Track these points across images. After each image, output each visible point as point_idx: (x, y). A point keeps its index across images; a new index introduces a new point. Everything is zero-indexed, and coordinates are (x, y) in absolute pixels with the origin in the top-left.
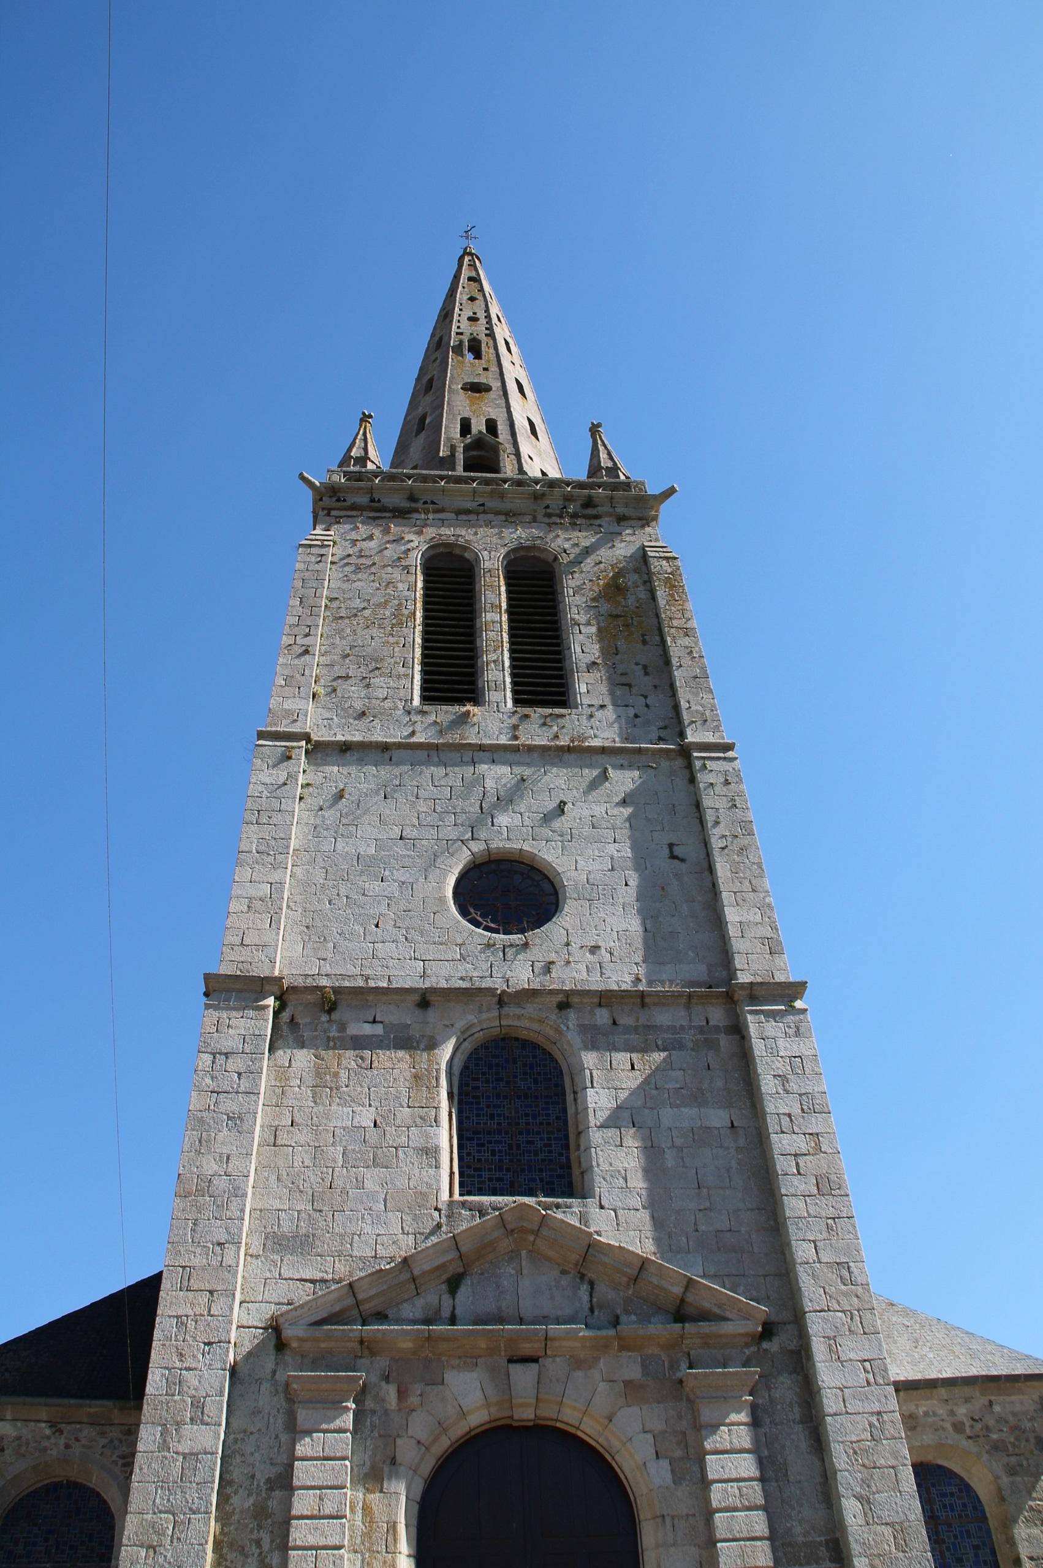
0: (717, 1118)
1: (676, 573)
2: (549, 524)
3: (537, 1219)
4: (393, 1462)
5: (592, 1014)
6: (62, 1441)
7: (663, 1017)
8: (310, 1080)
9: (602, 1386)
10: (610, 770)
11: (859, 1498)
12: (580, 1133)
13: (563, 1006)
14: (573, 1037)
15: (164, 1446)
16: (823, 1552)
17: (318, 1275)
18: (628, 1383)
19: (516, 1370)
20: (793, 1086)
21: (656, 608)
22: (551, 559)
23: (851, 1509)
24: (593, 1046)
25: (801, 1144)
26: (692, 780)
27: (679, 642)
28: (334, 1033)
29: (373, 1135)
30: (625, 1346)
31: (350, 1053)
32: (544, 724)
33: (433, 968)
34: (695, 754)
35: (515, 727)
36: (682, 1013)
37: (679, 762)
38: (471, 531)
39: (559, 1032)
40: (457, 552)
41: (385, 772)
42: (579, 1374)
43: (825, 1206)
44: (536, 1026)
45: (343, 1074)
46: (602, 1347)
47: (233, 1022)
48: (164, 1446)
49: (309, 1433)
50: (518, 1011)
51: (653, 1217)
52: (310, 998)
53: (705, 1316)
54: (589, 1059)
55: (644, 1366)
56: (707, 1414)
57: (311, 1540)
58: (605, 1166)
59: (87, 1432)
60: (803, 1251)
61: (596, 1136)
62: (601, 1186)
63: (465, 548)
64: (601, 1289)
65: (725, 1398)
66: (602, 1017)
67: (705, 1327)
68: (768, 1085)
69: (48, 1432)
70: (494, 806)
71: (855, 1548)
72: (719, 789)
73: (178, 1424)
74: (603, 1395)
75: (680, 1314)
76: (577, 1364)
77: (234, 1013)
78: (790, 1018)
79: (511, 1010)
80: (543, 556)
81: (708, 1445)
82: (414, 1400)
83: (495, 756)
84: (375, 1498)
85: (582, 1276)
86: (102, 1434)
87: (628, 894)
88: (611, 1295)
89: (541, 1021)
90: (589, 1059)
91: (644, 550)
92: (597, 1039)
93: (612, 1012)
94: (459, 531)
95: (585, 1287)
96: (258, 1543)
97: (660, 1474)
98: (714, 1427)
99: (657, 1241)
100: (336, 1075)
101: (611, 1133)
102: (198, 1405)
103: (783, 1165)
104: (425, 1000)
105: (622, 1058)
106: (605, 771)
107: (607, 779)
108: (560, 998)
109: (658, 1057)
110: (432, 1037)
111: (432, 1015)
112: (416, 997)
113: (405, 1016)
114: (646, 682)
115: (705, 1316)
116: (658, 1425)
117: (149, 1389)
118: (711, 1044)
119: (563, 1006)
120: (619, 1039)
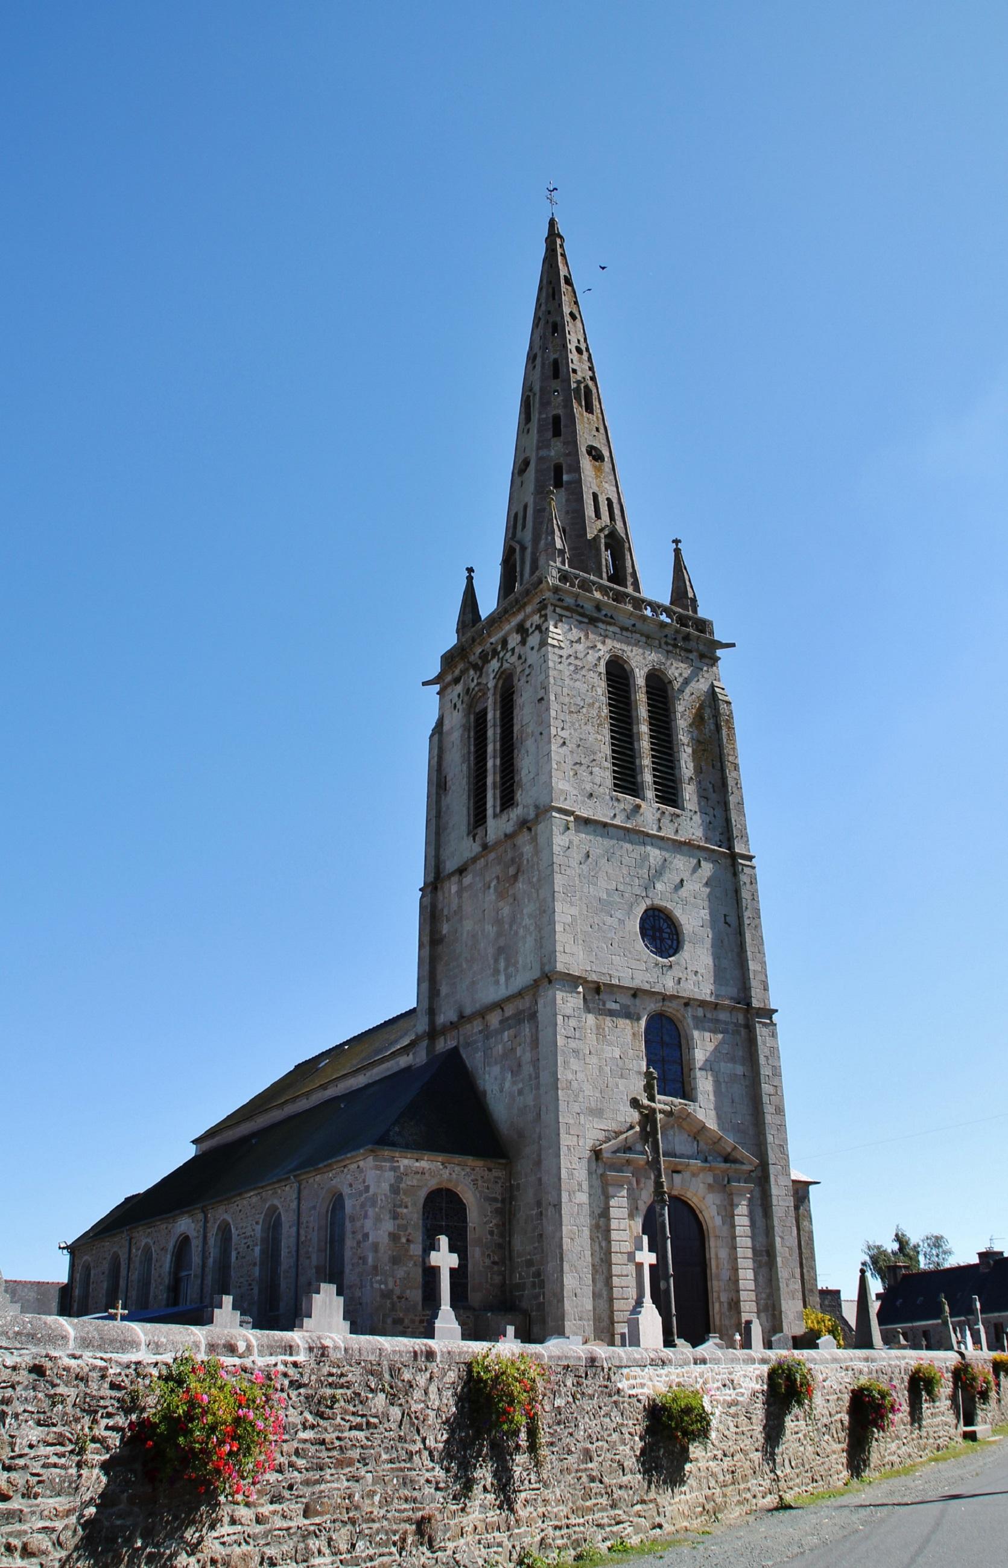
0: (740, 1070)
1: (731, 715)
2: (668, 652)
3: (686, 1114)
4: (637, 1208)
5: (696, 1010)
6: (447, 1172)
7: (723, 1016)
8: (594, 1031)
9: (701, 1185)
10: (702, 862)
11: (780, 1237)
12: (691, 1070)
13: (686, 1005)
14: (690, 1021)
15: (570, 1201)
16: (764, 1253)
17: (606, 1128)
18: (709, 1185)
19: (675, 1175)
20: (770, 1062)
21: (720, 739)
22: (666, 681)
23: (778, 1240)
24: (697, 1028)
25: (772, 1090)
26: (735, 874)
27: (732, 774)
28: (601, 1007)
29: (620, 1062)
30: (710, 1169)
31: (608, 1018)
32: (672, 821)
33: (637, 974)
34: (740, 861)
35: (659, 820)
36: (728, 1015)
37: (729, 861)
38: (630, 648)
39: (684, 1017)
40: (621, 662)
41: (607, 843)
42: (693, 1179)
43: (777, 1120)
44: (674, 1012)
45: (606, 1029)
46: (703, 1169)
47: (569, 999)
48: (570, 1201)
49: (613, 1197)
50: (670, 1004)
51: (717, 1114)
52: (591, 985)
53: (735, 1161)
54: (696, 1034)
55: (714, 1178)
56: (736, 1200)
57: (618, 1239)
58: (701, 1088)
59: (457, 1168)
60: (770, 1139)
61: (699, 1074)
62: (700, 1097)
63: (626, 662)
64: (701, 1143)
65: (742, 1195)
66: (700, 1012)
67: (737, 1166)
68: (762, 1060)
69: (441, 1167)
70: (654, 877)
71: (778, 1254)
72: (748, 885)
73: (574, 1192)
74: (702, 1189)
75: (727, 1159)
76: (694, 1175)
77: (568, 995)
78: (771, 1027)
79: (667, 1003)
80: (662, 677)
81: (736, 1213)
82: (642, 1185)
83: (653, 841)
84: (632, 1222)
85: (695, 1138)
86: (463, 1169)
87: (708, 942)
88: (705, 1147)
89: (678, 1011)
90: (696, 1034)
91: (714, 690)
92: (700, 1024)
93: (704, 1010)
94: (624, 647)
95: (696, 1143)
96: (598, 1237)
97: (718, 1221)
98: (737, 1206)
99: (719, 1125)
100: (604, 1029)
101: (704, 1073)
102: (580, 1185)
103: (765, 1099)
104: (636, 993)
105: (707, 1035)
106: (699, 861)
107: (700, 866)
108: (686, 1001)
109: (720, 1036)
110: (638, 1014)
111: (638, 1001)
112: (632, 992)
113: (626, 1000)
114: (714, 797)
115: (735, 1161)
116: (718, 1202)
117: (562, 1176)
118: (738, 1032)
119: (686, 1005)
120: (707, 1025)
